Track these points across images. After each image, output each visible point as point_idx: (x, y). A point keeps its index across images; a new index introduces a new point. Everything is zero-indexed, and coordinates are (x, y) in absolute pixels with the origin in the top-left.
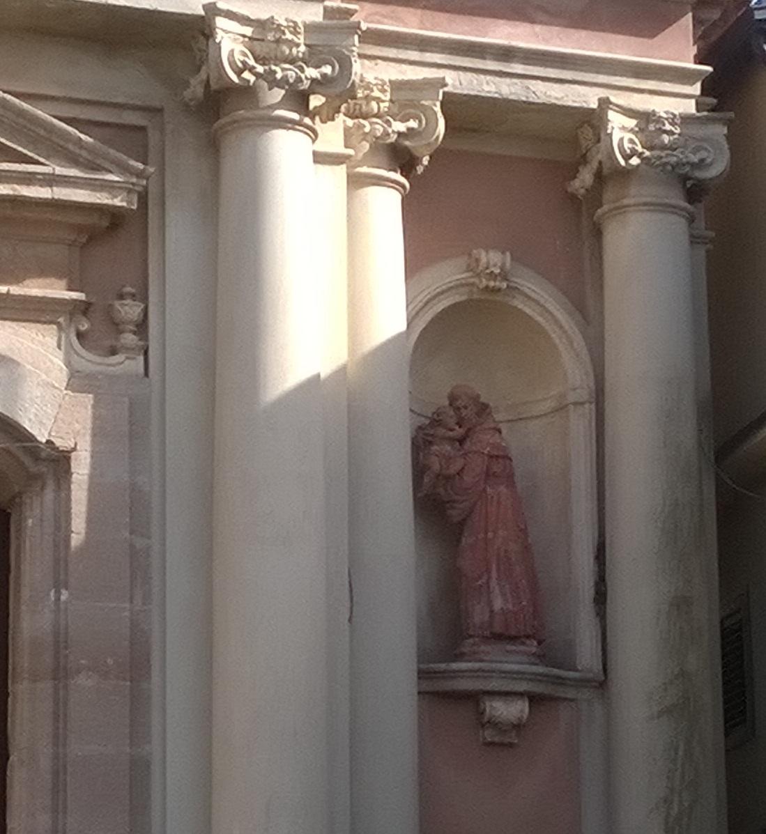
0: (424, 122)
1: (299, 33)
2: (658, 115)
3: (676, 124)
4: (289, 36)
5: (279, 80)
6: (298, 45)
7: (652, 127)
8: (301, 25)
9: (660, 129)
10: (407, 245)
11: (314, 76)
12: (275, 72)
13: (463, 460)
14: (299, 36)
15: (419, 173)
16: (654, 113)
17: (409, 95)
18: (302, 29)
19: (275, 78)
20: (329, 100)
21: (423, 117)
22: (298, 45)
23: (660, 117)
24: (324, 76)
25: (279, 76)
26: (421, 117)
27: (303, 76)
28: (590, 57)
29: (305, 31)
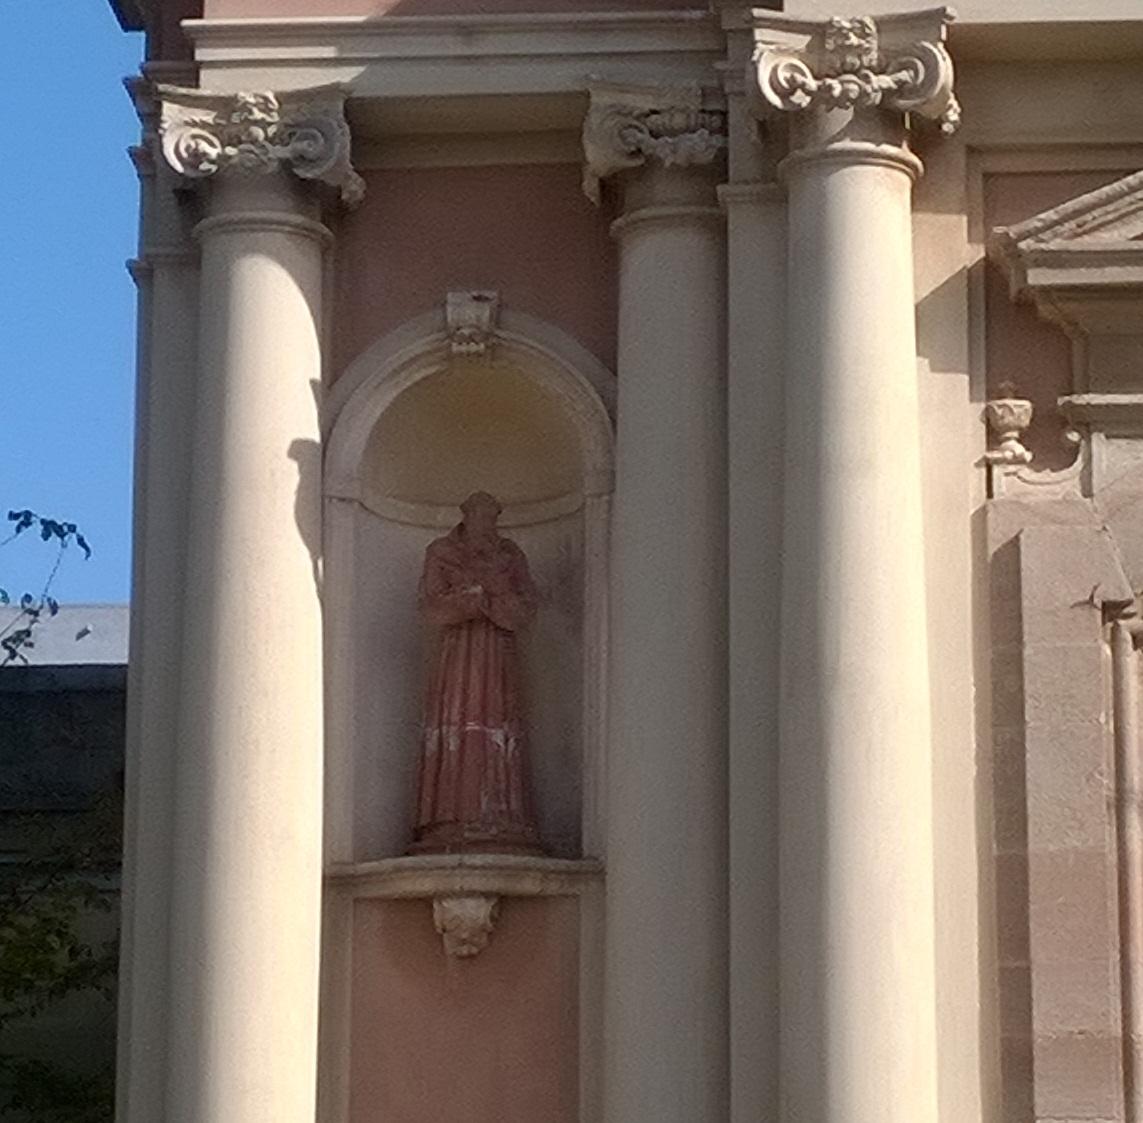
0: (921, 77)
1: (868, 35)
2: (243, 101)
3: (272, 110)
4: (854, 40)
5: (839, 97)
6: (868, 51)
7: (235, 118)
8: (868, 21)
9: (246, 119)
10: (323, 1005)
11: (885, 86)
12: (830, 88)
13: (152, 107)
14: (869, 39)
15: (1070, 436)
16: (234, 99)
17: (901, 39)
18: (874, 29)
19: (832, 96)
20: (827, 96)
21: (920, 64)
22: (868, 51)
23: (247, 103)
24: (901, 84)
25: (837, 92)
26: (916, 65)
27: (869, 88)
28: (215, 26)
29: (878, 31)
